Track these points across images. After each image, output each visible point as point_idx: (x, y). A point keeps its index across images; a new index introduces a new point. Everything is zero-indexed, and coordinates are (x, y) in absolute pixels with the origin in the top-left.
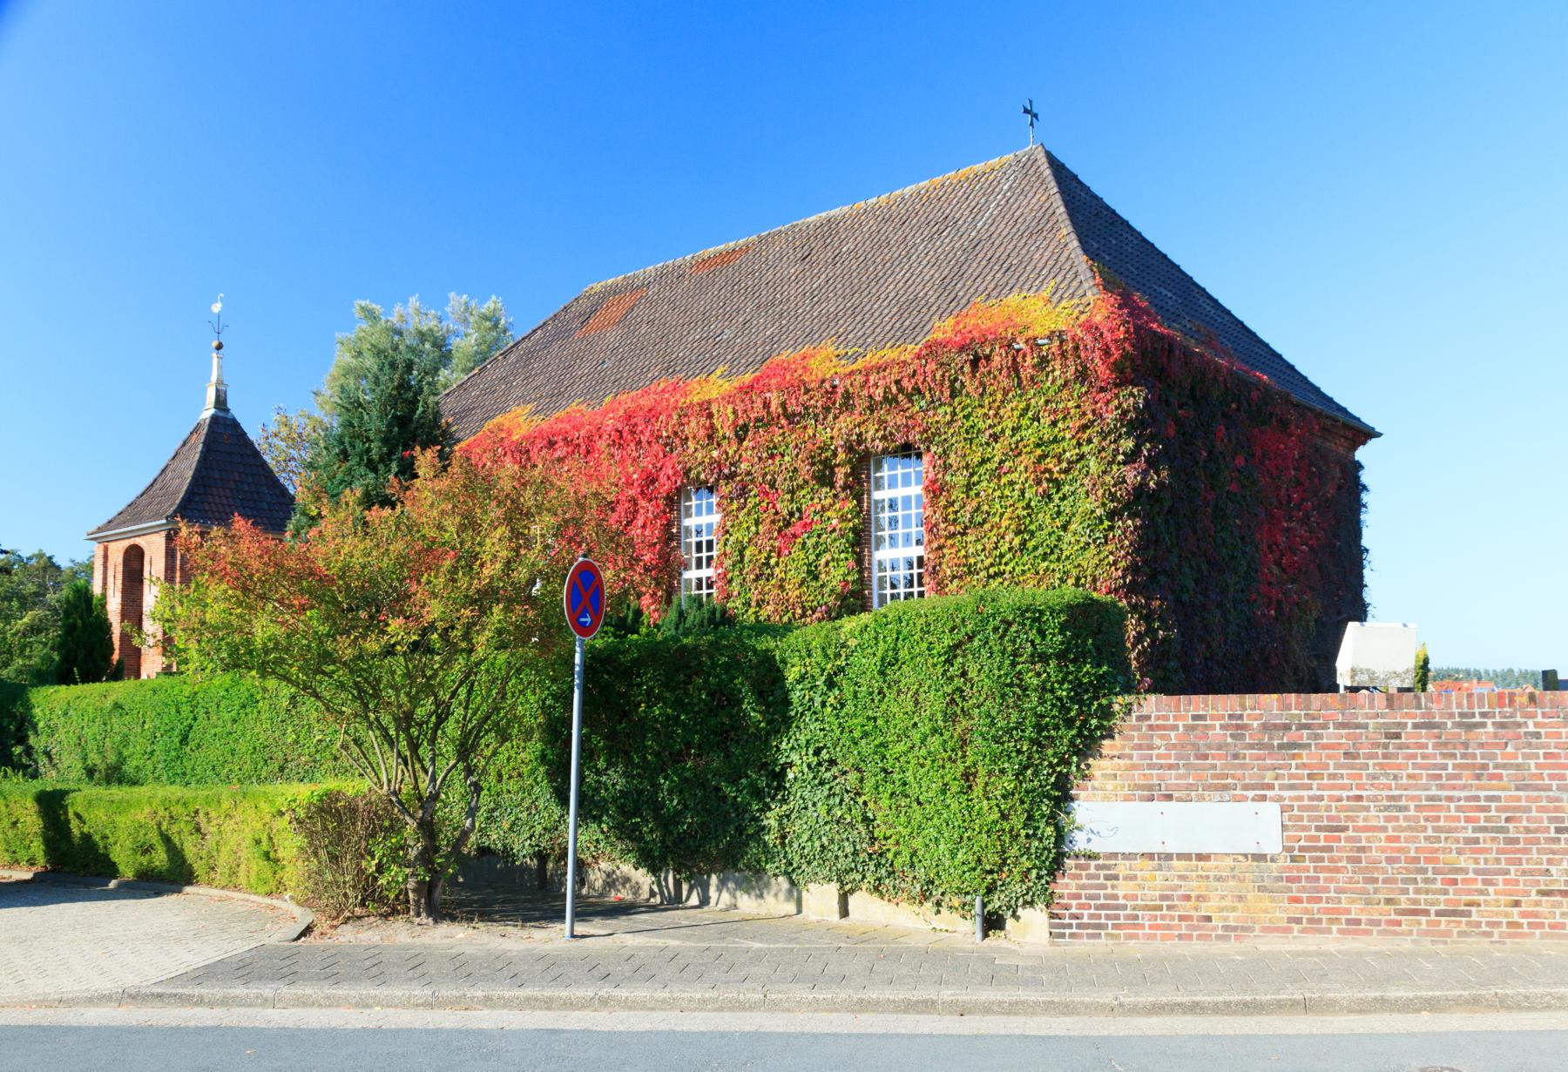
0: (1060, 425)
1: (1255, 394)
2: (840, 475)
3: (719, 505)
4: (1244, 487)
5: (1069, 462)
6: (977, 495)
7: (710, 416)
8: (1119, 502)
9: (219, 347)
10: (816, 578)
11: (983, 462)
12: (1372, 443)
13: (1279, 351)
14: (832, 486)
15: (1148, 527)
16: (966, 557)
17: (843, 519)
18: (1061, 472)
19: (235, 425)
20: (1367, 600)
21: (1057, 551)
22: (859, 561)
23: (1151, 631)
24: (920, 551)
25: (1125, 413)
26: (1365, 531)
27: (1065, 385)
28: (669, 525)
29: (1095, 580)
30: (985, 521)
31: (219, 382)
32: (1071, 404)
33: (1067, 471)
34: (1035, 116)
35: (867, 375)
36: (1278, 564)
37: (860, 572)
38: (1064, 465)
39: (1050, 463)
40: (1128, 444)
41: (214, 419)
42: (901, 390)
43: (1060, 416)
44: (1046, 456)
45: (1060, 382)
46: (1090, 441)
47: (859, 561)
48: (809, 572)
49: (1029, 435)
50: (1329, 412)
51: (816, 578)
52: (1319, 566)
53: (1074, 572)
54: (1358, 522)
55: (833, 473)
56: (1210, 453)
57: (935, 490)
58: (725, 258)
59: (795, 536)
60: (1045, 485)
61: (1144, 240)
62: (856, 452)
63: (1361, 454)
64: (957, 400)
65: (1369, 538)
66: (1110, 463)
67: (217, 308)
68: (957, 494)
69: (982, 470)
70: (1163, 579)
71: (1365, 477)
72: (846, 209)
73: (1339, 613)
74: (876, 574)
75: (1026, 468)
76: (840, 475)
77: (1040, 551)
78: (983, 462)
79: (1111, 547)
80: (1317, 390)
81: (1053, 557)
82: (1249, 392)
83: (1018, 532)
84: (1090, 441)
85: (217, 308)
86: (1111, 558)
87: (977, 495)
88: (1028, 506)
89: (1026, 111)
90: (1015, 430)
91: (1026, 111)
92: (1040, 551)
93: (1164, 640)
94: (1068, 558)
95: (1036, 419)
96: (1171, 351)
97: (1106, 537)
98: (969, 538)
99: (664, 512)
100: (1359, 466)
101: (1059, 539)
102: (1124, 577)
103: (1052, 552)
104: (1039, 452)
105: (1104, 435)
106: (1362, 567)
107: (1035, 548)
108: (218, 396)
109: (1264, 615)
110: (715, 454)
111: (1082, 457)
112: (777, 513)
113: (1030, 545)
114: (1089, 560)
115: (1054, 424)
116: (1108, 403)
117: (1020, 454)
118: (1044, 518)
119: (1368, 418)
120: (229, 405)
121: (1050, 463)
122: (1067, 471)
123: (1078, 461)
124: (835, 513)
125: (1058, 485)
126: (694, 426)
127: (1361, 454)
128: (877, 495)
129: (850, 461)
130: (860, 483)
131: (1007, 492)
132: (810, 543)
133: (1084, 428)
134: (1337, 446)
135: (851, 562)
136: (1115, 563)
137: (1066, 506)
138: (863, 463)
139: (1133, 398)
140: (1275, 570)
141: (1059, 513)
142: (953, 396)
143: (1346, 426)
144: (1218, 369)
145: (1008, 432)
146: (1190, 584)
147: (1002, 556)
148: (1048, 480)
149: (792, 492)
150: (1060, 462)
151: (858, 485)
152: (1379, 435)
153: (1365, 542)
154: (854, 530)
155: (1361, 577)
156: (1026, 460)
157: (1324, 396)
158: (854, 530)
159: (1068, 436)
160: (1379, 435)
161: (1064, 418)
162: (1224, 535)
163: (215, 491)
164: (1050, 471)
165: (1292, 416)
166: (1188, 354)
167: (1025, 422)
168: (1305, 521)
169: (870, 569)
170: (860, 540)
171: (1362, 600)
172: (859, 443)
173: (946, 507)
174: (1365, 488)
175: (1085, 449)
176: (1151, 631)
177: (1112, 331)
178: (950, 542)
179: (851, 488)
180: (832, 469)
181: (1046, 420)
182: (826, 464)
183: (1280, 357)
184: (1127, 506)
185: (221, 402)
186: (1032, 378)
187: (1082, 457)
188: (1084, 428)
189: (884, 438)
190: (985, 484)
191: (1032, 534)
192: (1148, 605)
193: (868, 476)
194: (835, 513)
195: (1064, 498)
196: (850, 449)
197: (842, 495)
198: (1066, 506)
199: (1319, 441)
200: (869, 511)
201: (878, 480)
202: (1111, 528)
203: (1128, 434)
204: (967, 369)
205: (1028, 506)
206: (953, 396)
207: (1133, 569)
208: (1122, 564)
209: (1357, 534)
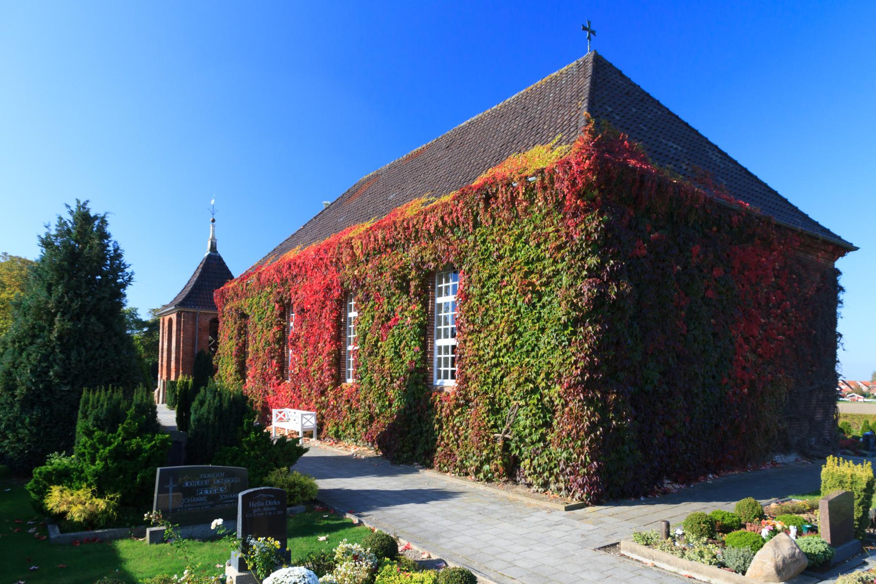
0: (542, 247)
1: (735, 218)
3: (356, 306)
5: (549, 278)
6: (487, 302)
7: (352, 248)
8: (580, 310)
9: (213, 221)
10: (400, 357)
11: (490, 277)
12: (850, 255)
13: (775, 189)
14: (407, 293)
15: (609, 330)
16: (478, 350)
17: (413, 317)
18: (542, 285)
20: (839, 372)
26: (839, 321)
27: (548, 214)
28: (340, 316)
31: (213, 238)
34: (593, 32)
35: (426, 215)
38: (544, 279)
39: (534, 278)
40: (592, 261)
41: (209, 256)
42: (444, 223)
43: (543, 239)
44: (532, 272)
46: (563, 260)
48: (395, 353)
49: (522, 255)
50: (809, 231)
51: (400, 357)
53: (545, 368)
55: (408, 286)
56: (685, 268)
57: (465, 297)
58: (418, 153)
59: (390, 328)
61: (670, 113)
62: (423, 270)
63: (840, 264)
64: (477, 230)
65: (841, 327)
66: (576, 278)
67: (213, 202)
70: (622, 375)
71: (842, 281)
72: (480, 115)
73: (812, 384)
74: (437, 356)
75: (517, 283)
77: (525, 349)
78: (490, 277)
80: (805, 217)
83: (509, 333)
84: (563, 260)
86: (574, 358)
88: (519, 312)
89: (585, 29)
90: (513, 251)
91: (585, 29)
92: (525, 349)
93: (617, 429)
94: (542, 355)
95: (526, 242)
96: (642, 182)
97: (569, 340)
98: (482, 335)
99: (336, 309)
100: (838, 273)
101: (537, 339)
102: (582, 375)
103: (533, 350)
104: (526, 269)
105: (574, 253)
107: (522, 346)
110: (356, 272)
111: (557, 273)
113: (518, 343)
114: (556, 359)
115: (538, 246)
116: (577, 225)
117: (513, 271)
119: (847, 237)
120: (218, 249)
121: (534, 278)
122: (547, 284)
123: (554, 276)
124: (408, 313)
125: (540, 296)
126: (345, 258)
127: (840, 264)
128: (439, 300)
129: (419, 275)
130: (426, 291)
131: (506, 301)
132: (396, 332)
133: (559, 248)
134: (820, 258)
135: (417, 348)
136: (576, 362)
137: (545, 312)
139: (594, 223)
140: (751, 357)
141: (539, 319)
142: (475, 227)
143: (826, 242)
145: (508, 253)
147: (500, 350)
148: (533, 292)
149: (389, 298)
150: (541, 276)
152: (856, 249)
153: (839, 329)
154: (420, 326)
155: (834, 355)
156: (517, 277)
157: (811, 221)
158: (420, 326)
159: (548, 256)
160: (856, 249)
161: (545, 241)
164: (532, 284)
166: (661, 185)
167: (519, 245)
169: (432, 353)
170: (426, 331)
172: (423, 263)
174: (842, 289)
177: (578, 164)
178: (470, 337)
179: (419, 295)
182: (404, 278)
183: (776, 193)
184: (589, 314)
185: (213, 248)
187: (557, 273)
188: (559, 248)
189: (434, 260)
190: (492, 294)
191: (521, 335)
192: (604, 398)
193: (433, 287)
194: (408, 313)
195: (543, 307)
196: (418, 268)
197: (413, 301)
198: (545, 312)
200: (433, 312)
202: (574, 333)
203: (593, 253)
205: (519, 312)
206: (475, 227)
207: (590, 368)
208: (581, 364)
209: (834, 324)
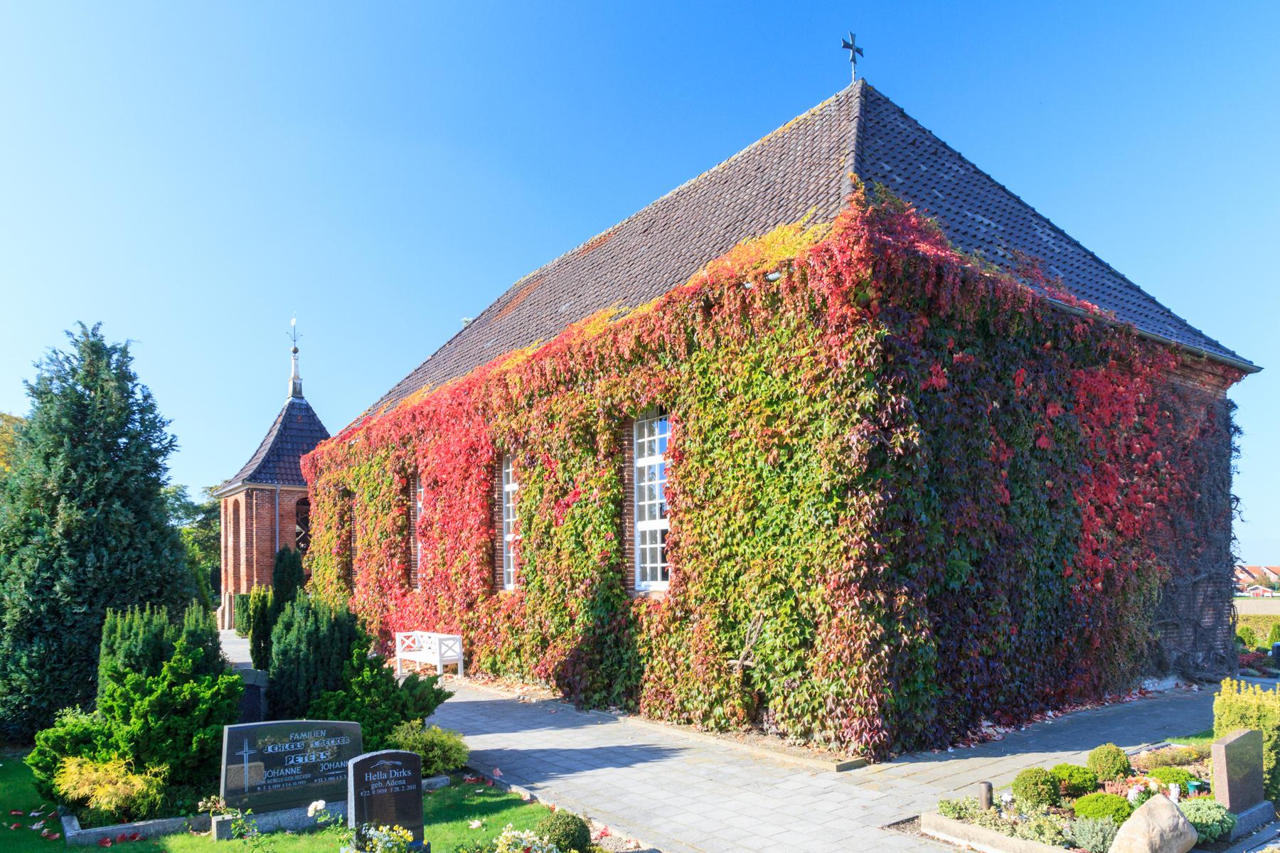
0: (792, 378)
1: (1079, 327)
2: (603, 440)
3: (515, 473)
4: (1058, 441)
6: (712, 464)
7: (506, 386)
8: (849, 472)
9: (296, 351)
11: (715, 425)
12: (1249, 379)
14: (595, 452)
16: (700, 535)
17: (604, 488)
18: (793, 435)
19: (308, 408)
21: (787, 531)
22: (620, 533)
23: (891, 635)
24: (664, 524)
25: (860, 359)
26: (1235, 478)
27: (799, 328)
29: (824, 570)
30: (718, 493)
31: (296, 377)
32: (804, 351)
33: (801, 434)
34: (859, 51)
36: (1111, 527)
37: (621, 543)
38: (796, 427)
39: (781, 425)
43: (792, 366)
44: (778, 417)
45: (793, 324)
47: (620, 533)
49: (762, 392)
51: (585, 549)
52: (1172, 523)
53: (802, 559)
54: (1228, 468)
56: (1005, 403)
59: (568, 506)
60: (775, 452)
65: (1238, 487)
66: (843, 424)
68: (693, 463)
69: (714, 435)
71: (1238, 418)
74: (638, 546)
76: (603, 440)
77: (770, 532)
78: (715, 425)
79: (842, 530)
81: (783, 539)
82: (1072, 325)
84: (823, 397)
85: (293, 322)
86: (843, 544)
87: (712, 464)
88: (759, 477)
89: (847, 46)
90: (748, 385)
91: (847, 46)
93: (912, 647)
96: (940, 277)
98: (706, 513)
100: (1231, 406)
102: (857, 568)
103: (782, 533)
104: (768, 411)
105: (839, 387)
106: (1229, 518)
107: (766, 528)
108: (295, 388)
109: (1083, 590)
111: (815, 417)
112: (557, 482)
113: (760, 523)
118: (772, 492)
121: (781, 425)
122: (801, 434)
123: (811, 421)
127: (1233, 393)
133: (817, 379)
134: (1203, 385)
136: (846, 550)
138: (623, 428)
141: (790, 487)
144: (1018, 299)
145: (740, 389)
146: (966, 566)
147: (733, 535)
149: (565, 461)
151: (620, 448)
152: (1259, 369)
156: (755, 424)
159: (801, 391)
160: (1259, 369)
162: (1025, 501)
163: (286, 459)
165: (1137, 351)
167: (757, 376)
168: (1153, 473)
170: (620, 510)
171: (1229, 554)
173: (684, 477)
175: (819, 407)
176: (891, 635)
180: (594, 435)
181: (778, 373)
182: (587, 428)
184: (863, 478)
185: (297, 392)
186: (765, 324)
187: (815, 417)
188: (817, 379)
190: (718, 451)
191: (763, 511)
193: (631, 444)
194: (592, 478)
195: (796, 468)
196: (609, 415)
199: (1177, 380)
201: (641, 446)
202: (842, 506)
203: (868, 385)
204: (699, 318)
205: (759, 477)
207: (871, 558)
208: (854, 553)
209: (1227, 482)
